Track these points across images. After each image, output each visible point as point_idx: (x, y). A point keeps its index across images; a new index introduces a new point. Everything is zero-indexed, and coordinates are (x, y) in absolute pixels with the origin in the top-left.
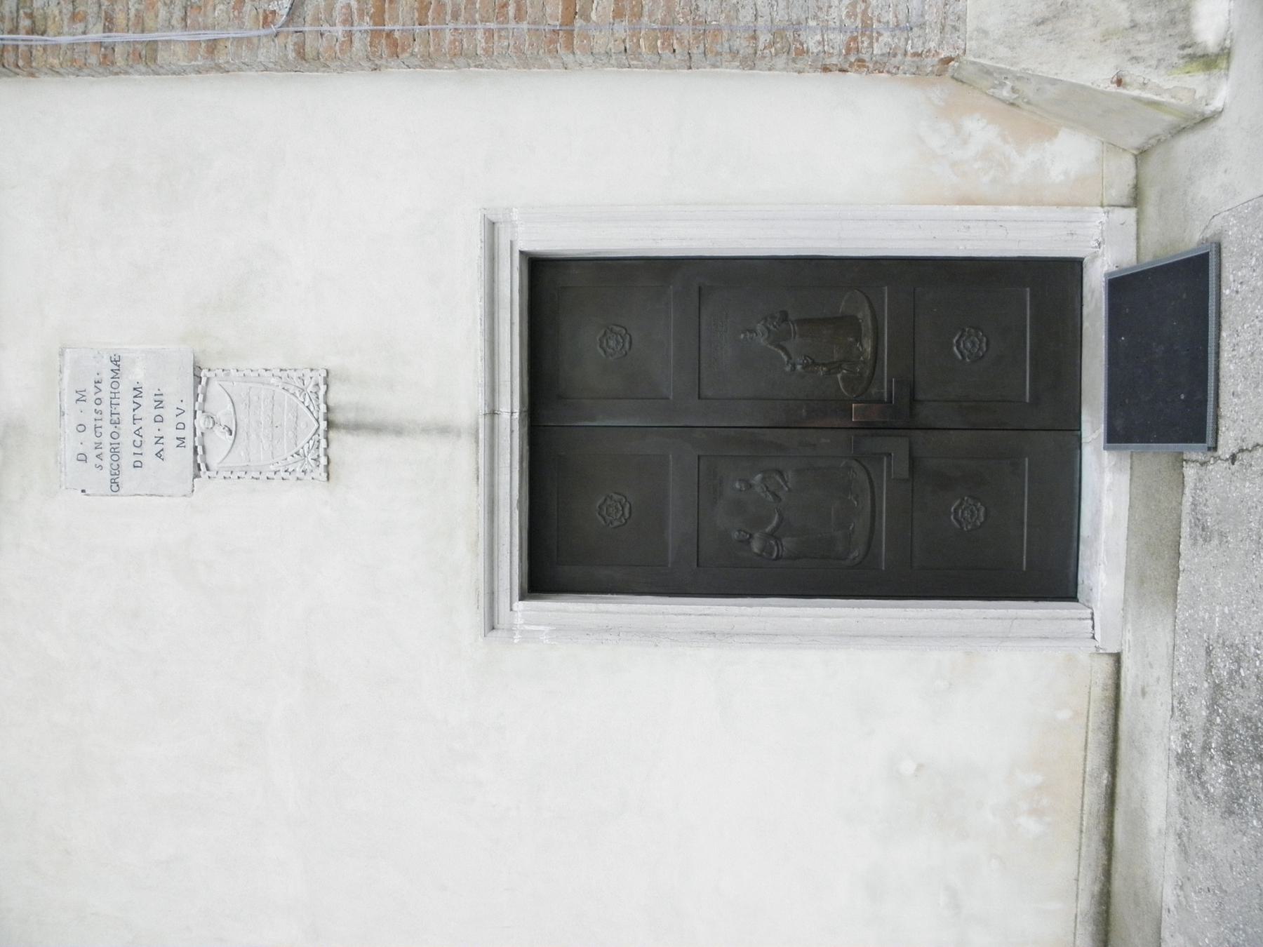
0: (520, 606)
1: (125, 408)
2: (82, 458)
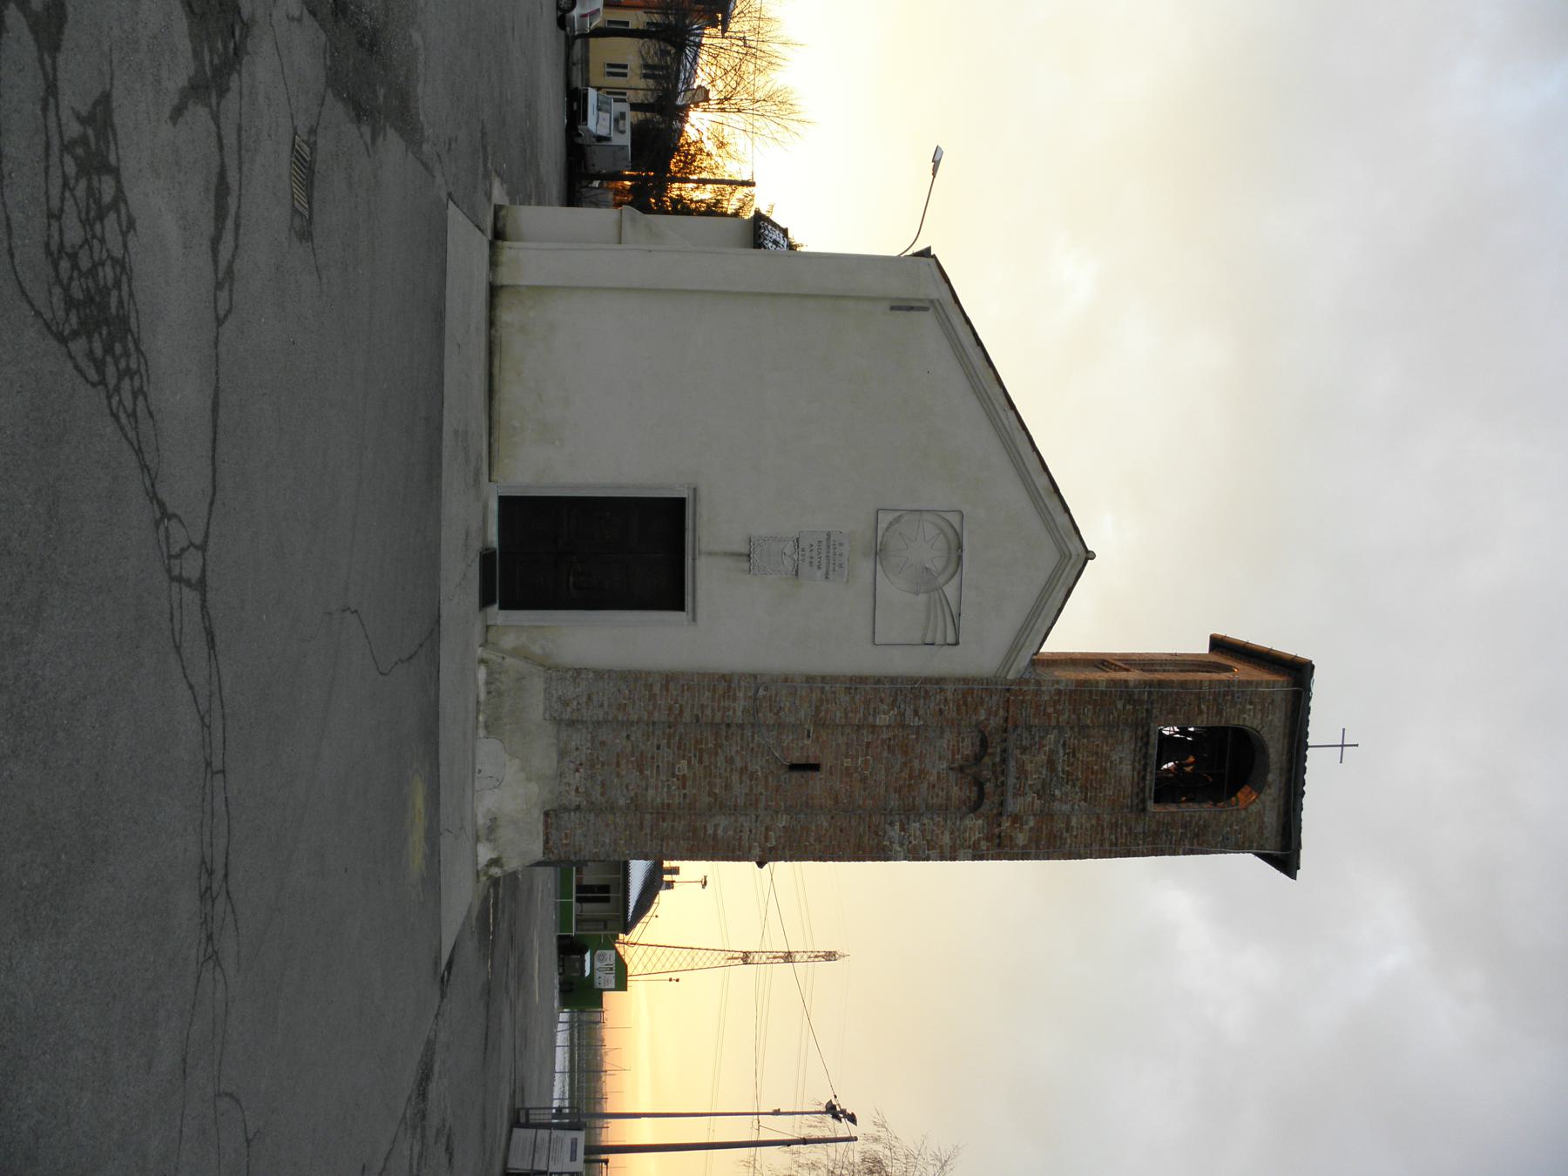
0: (686, 496)
1: (824, 561)
2: (841, 544)
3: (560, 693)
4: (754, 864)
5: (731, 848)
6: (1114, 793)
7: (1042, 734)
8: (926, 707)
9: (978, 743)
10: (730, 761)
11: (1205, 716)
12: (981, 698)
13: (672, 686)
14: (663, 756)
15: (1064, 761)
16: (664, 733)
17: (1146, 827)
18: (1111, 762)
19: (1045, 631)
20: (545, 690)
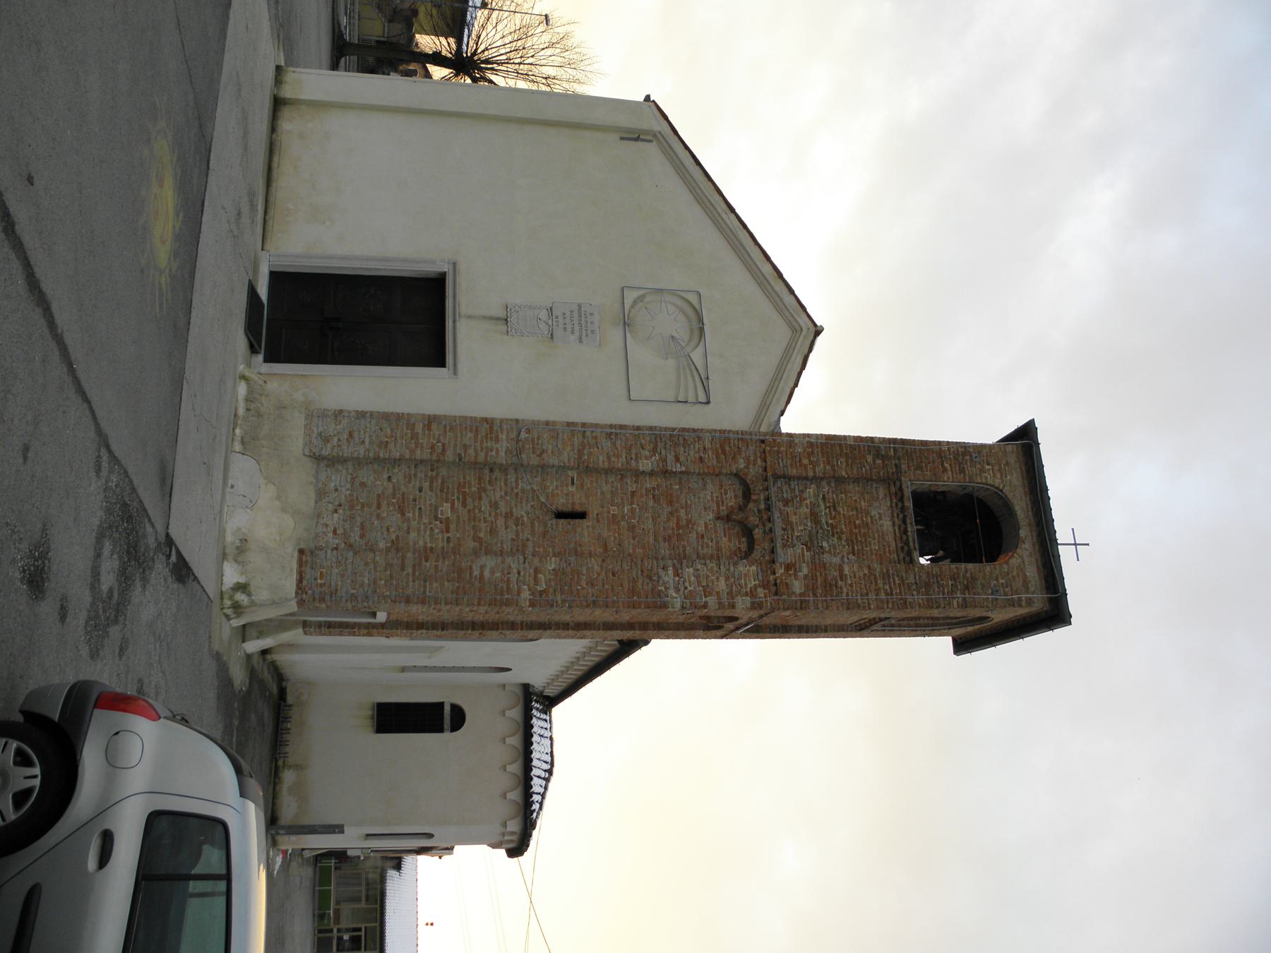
0: (446, 270)
2: (591, 314)
3: (321, 429)
4: (502, 852)
5: (499, 591)
6: (879, 548)
7: (801, 488)
8: (687, 454)
9: (741, 495)
10: (495, 505)
11: (950, 473)
12: (738, 447)
13: (434, 426)
14: (425, 497)
15: (826, 514)
16: (426, 476)
17: (917, 578)
18: (871, 517)
19: (788, 393)
20: (305, 426)
